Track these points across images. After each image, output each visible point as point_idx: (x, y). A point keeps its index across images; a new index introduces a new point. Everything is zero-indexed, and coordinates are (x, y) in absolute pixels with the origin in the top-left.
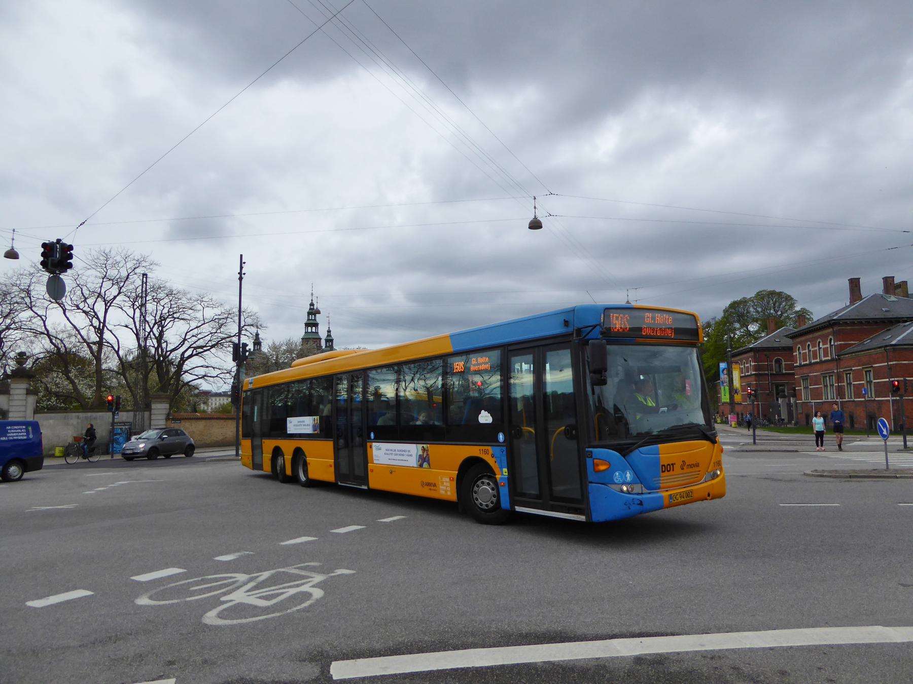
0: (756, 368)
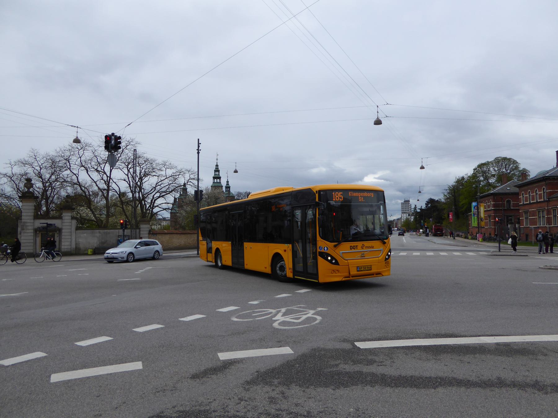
0: (494, 206)
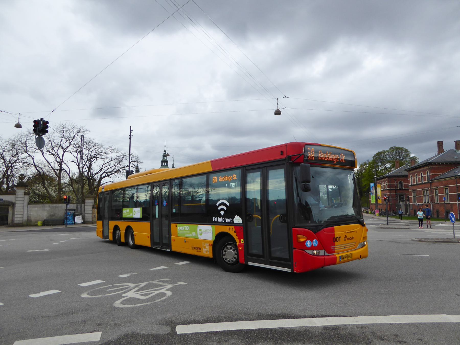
0: (389, 186)
